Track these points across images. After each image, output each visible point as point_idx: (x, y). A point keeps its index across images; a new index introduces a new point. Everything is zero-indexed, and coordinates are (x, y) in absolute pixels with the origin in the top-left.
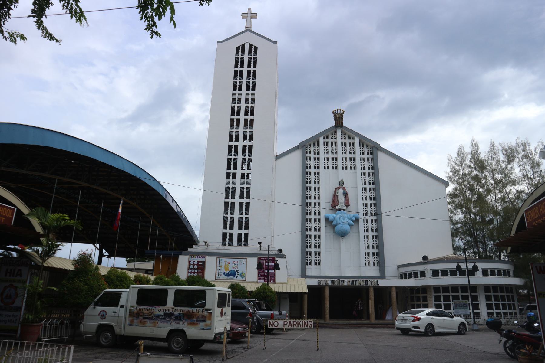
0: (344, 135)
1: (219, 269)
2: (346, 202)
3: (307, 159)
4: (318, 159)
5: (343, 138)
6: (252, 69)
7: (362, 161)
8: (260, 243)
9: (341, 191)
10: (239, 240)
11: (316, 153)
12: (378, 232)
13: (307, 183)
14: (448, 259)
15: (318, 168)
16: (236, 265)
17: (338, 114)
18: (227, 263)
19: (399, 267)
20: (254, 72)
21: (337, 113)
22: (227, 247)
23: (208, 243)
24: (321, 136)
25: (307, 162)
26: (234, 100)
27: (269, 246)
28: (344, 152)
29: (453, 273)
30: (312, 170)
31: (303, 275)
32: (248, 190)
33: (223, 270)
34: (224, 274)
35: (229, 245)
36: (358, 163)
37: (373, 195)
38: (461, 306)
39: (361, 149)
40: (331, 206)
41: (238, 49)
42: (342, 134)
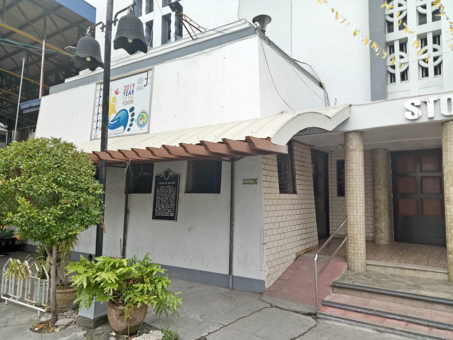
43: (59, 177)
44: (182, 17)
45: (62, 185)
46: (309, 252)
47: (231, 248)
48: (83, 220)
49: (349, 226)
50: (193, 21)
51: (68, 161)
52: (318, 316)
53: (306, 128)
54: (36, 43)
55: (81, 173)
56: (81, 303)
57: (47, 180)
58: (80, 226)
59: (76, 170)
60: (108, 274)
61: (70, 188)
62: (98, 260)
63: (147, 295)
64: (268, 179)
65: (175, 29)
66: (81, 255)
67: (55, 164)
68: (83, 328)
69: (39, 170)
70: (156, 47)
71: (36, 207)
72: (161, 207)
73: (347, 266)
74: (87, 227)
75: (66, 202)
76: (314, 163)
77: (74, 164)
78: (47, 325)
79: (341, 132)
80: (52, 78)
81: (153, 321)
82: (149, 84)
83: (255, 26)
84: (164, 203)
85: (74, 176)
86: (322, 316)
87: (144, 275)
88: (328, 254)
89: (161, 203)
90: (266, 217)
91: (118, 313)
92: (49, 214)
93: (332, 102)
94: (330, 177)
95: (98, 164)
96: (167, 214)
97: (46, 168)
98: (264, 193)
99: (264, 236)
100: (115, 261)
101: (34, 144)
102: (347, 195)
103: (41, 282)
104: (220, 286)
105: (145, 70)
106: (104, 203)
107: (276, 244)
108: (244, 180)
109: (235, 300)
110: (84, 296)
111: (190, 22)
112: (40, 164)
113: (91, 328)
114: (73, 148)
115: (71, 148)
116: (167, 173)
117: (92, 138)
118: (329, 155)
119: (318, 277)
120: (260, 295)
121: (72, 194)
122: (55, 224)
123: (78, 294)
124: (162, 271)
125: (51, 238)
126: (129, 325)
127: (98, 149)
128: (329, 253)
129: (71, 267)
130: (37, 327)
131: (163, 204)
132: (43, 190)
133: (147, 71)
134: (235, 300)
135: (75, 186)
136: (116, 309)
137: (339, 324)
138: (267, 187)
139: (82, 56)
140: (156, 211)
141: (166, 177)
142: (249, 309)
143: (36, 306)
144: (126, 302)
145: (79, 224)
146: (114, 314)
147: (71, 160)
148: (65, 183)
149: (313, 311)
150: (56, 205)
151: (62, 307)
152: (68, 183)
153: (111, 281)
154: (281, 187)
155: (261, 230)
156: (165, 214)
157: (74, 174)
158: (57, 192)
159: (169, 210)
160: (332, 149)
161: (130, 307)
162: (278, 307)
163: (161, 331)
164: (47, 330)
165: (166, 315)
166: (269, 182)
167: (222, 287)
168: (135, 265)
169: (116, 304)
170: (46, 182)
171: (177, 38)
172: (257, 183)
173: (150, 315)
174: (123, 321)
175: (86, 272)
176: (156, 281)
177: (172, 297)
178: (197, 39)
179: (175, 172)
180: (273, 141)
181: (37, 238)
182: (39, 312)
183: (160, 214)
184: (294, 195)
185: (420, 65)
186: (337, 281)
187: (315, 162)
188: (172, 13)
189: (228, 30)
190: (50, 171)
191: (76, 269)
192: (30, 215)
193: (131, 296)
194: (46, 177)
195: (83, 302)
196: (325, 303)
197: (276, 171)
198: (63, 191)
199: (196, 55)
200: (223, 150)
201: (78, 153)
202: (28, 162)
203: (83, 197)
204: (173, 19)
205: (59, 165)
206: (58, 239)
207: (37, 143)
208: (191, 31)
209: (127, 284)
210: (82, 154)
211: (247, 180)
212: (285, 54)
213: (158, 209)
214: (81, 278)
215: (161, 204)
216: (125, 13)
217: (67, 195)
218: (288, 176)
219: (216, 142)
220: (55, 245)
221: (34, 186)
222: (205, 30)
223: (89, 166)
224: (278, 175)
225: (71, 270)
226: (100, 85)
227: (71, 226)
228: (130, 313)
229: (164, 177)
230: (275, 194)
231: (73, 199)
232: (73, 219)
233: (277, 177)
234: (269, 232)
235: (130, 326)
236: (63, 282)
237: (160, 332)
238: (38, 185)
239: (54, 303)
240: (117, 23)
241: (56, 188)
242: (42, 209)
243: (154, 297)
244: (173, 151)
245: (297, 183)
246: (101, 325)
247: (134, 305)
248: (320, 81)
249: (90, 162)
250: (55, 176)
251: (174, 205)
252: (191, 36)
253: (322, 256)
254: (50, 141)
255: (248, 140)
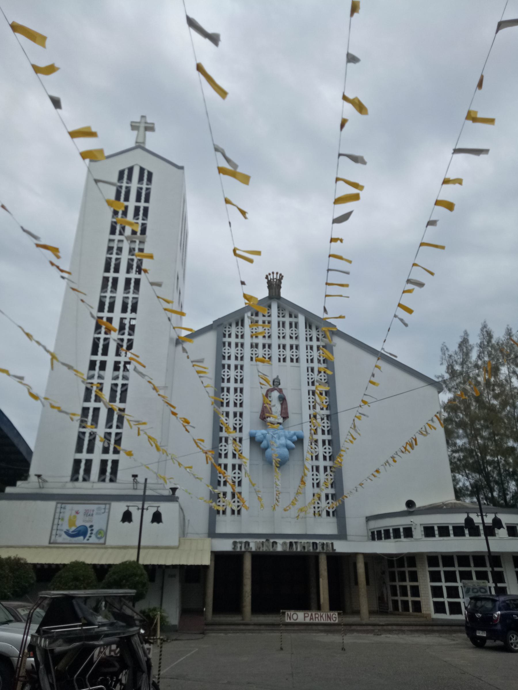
0: (282, 310)
1: (58, 525)
2: (283, 411)
3: (224, 346)
4: (242, 345)
5: (281, 315)
6: (142, 204)
7: (309, 350)
8: (135, 476)
9: (275, 394)
10: (103, 471)
11: (240, 337)
12: (332, 434)
13: (223, 382)
14: (449, 507)
15: (242, 358)
16: (89, 515)
17: (273, 279)
18: (74, 513)
19: (369, 519)
20: (146, 210)
21: (272, 278)
22: (80, 484)
23: (42, 477)
24: (246, 312)
25: (225, 349)
26: (110, 249)
27: (146, 480)
28: (281, 336)
29: (459, 531)
30: (233, 362)
31: (212, 534)
32: (124, 389)
33: (65, 527)
34: (67, 533)
35: (84, 480)
36: (303, 353)
37: (329, 453)
38: (475, 590)
39: (308, 333)
40: (260, 418)
41: (121, 173)
42: (279, 310)
70: (490, 542)
185: (321, 502)
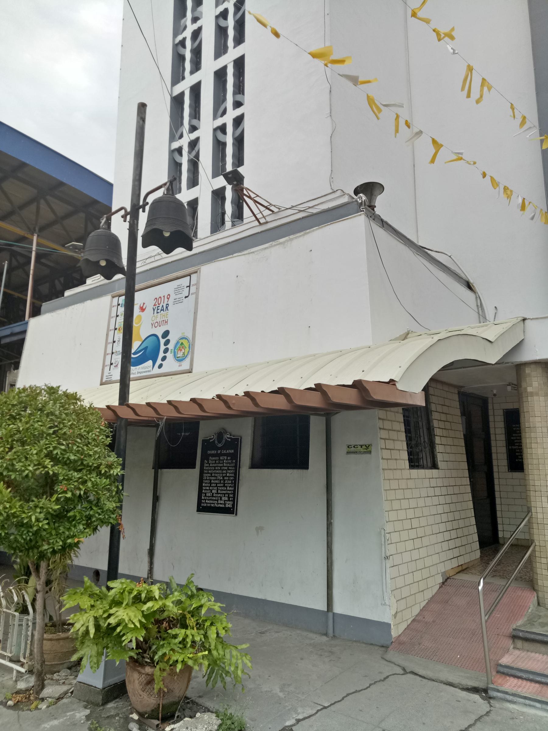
43: (55, 448)
44: (243, 191)
45: (60, 462)
46: (465, 572)
47: (329, 564)
48: (90, 519)
49: (535, 526)
50: (260, 197)
51: (70, 423)
52: (492, 693)
53: (453, 362)
54: (22, 239)
55: (88, 442)
56: (84, 662)
57: (36, 454)
58: (85, 529)
59: (81, 436)
60: (128, 611)
61: (72, 465)
62: (111, 586)
63: (191, 650)
64: (390, 445)
65: (232, 209)
66: (84, 576)
67: (50, 428)
68: (85, 703)
69: (25, 439)
71: (18, 498)
72: (211, 492)
73: (536, 598)
74: (95, 529)
75: (65, 489)
76: (465, 415)
77: (79, 426)
78: (28, 696)
79: (510, 364)
80: (45, 289)
81: (201, 694)
82: (192, 294)
83: (358, 200)
84: (217, 485)
85: (78, 447)
86: (499, 695)
87: (186, 613)
88: (500, 575)
89: (211, 485)
90: (388, 511)
91: (143, 679)
92: (38, 510)
93: (490, 313)
94: (493, 437)
95: (114, 423)
96: (221, 504)
97: (35, 435)
98: (383, 469)
99: (387, 544)
100: (140, 589)
101: (19, 397)
102: (528, 472)
103: (21, 620)
104: (311, 631)
105: (186, 274)
106: (123, 489)
107: (407, 557)
108: (348, 447)
109: (340, 658)
110: (88, 649)
111: (256, 199)
112: (27, 429)
113: (97, 705)
114: (78, 402)
115: (75, 401)
116: (220, 435)
117: (104, 381)
118: (490, 401)
119: (486, 621)
120: (383, 649)
121: (74, 476)
122: (46, 527)
123: (79, 645)
124: (217, 607)
125: (40, 549)
126: (162, 702)
127: (115, 401)
128: (501, 574)
129: (69, 597)
130: (11, 700)
131: (214, 487)
132: (30, 471)
133: (189, 275)
134: (340, 658)
135: (79, 463)
136: (140, 673)
137: (532, 711)
138: (387, 459)
139: (93, 258)
140: (203, 498)
141: (220, 442)
142: (366, 676)
143: (11, 660)
144: (157, 661)
145: (83, 525)
146: (137, 682)
147: (74, 420)
148: (64, 458)
149: (481, 685)
150: (48, 494)
151: (52, 665)
152: (68, 458)
153: (133, 623)
154: (411, 457)
155: (380, 533)
156: (218, 504)
157: (79, 443)
158: (51, 473)
159: (224, 496)
160: (495, 392)
161: (164, 670)
162: (416, 674)
163: (214, 715)
164: (27, 706)
165: (224, 687)
166: (390, 449)
167: (316, 633)
168: (173, 597)
169: (140, 664)
170: (35, 457)
171: (235, 223)
172: (370, 452)
173: (195, 683)
174: (152, 693)
175: (92, 606)
176: (207, 624)
177: (234, 653)
178: (267, 223)
179: (233, 433)
180: (400, 386)
181: (17, 548)
182: (15, 672)
183: (210, 503)
184: (435, 471)
186: (520, 626)
187: (465, 413)
188: (226, 186)
189: (316, 207)
190: (43, 440)
191: (78, 601)
192: (10, 512)
193: (166, 650)
194: (35, 449)
195: (88, 659)
196: (502, 670)
197: (402, 432)
198: (61, 470)
199: (265, 248)
200: (315, 401)
201: (85, 408)
202: (9, 425)
203: (91, 480)
204: (229, 194)
205: (56, 429)
206: (51, 550)
207: (24, 395)
208: (256, 211)
209: (159, 627)
210: (91, 411)
211: (354, 447)
212: (408, 239)
213: (206, 495)
214: (85, 618)
215: (210, 486)
216: (159, 194)
217: (66, 478)
218: (422, 438)
219: (302, 388)
220: (45, 559)
221: (17, 465)
222: (279, 209)
223: (101, 429)
224: (406, 436)
225: (69, 603)
226: (118, 298)
227: (71, 530)
228: (163, 680)
229: (216, 442)
230: (401, 469)
231: (76, 484)
232: (75, 516)
233: (403, 441)
234: (395, 537)
235: (162, 704)
236: (55, 619)
237: (213, 716)
238: (23, 462)
239: (39, 658)
240: (147, 208)
241: (49, 466)
242: (28, 501)
243: (204, 653)
244: (234, 404)
245: (438, 451)
246: (115, 698)
247: (171, 666)
248: (467, 279)
249: (103, 423)
250: (49, 447)
251: (232, 489)
252: (257, 219)
253: (488, 580)
254: (43, 391)
255: (358, 385)
